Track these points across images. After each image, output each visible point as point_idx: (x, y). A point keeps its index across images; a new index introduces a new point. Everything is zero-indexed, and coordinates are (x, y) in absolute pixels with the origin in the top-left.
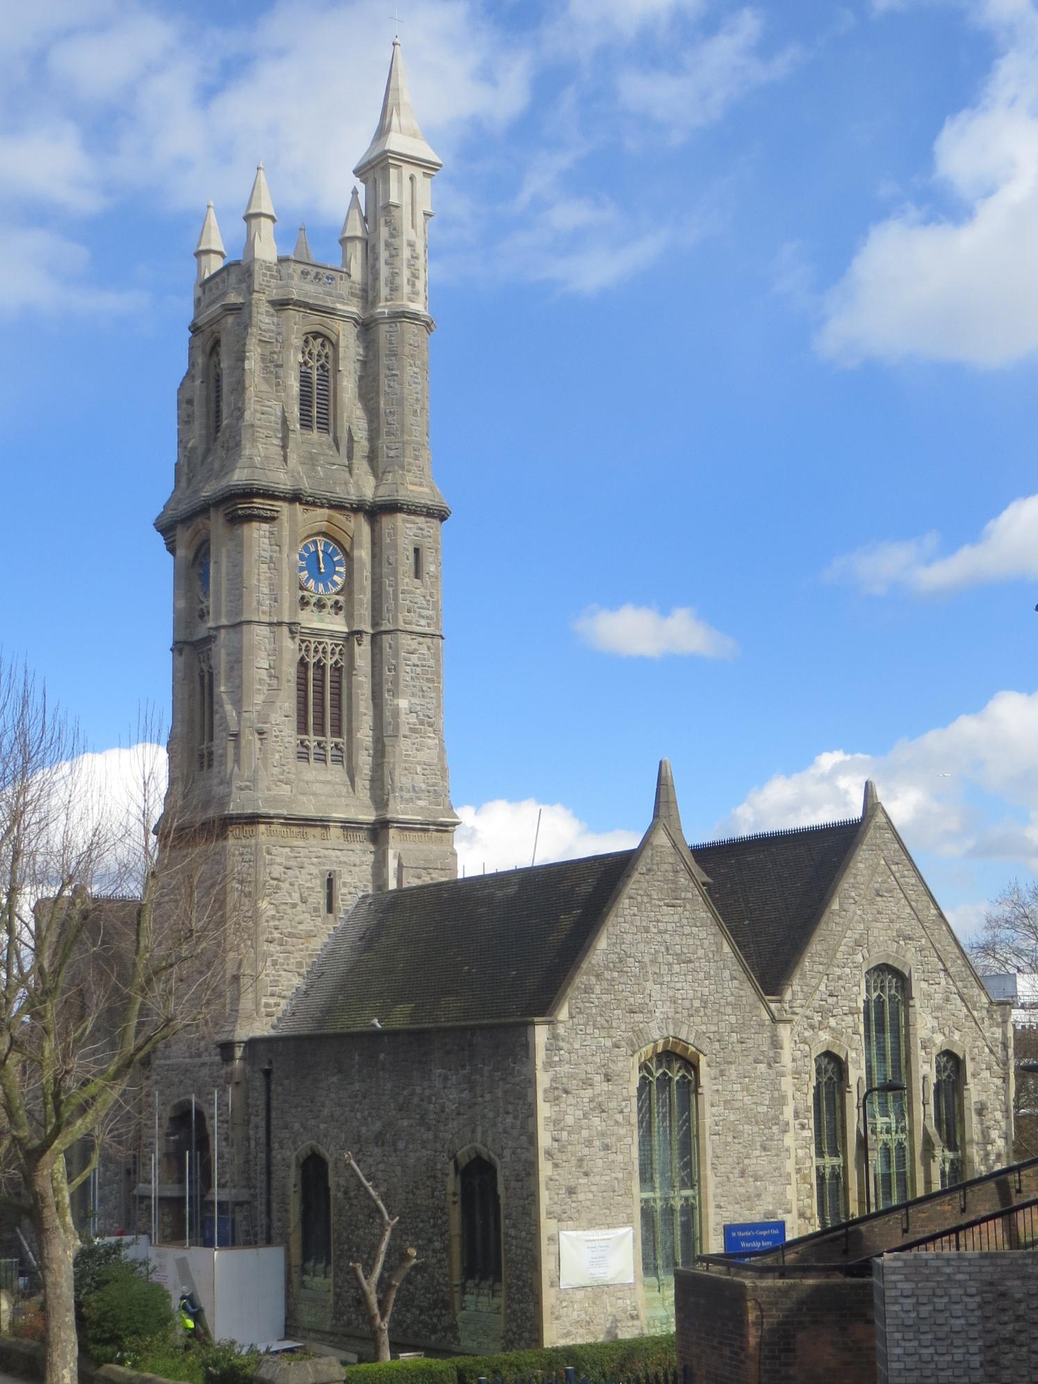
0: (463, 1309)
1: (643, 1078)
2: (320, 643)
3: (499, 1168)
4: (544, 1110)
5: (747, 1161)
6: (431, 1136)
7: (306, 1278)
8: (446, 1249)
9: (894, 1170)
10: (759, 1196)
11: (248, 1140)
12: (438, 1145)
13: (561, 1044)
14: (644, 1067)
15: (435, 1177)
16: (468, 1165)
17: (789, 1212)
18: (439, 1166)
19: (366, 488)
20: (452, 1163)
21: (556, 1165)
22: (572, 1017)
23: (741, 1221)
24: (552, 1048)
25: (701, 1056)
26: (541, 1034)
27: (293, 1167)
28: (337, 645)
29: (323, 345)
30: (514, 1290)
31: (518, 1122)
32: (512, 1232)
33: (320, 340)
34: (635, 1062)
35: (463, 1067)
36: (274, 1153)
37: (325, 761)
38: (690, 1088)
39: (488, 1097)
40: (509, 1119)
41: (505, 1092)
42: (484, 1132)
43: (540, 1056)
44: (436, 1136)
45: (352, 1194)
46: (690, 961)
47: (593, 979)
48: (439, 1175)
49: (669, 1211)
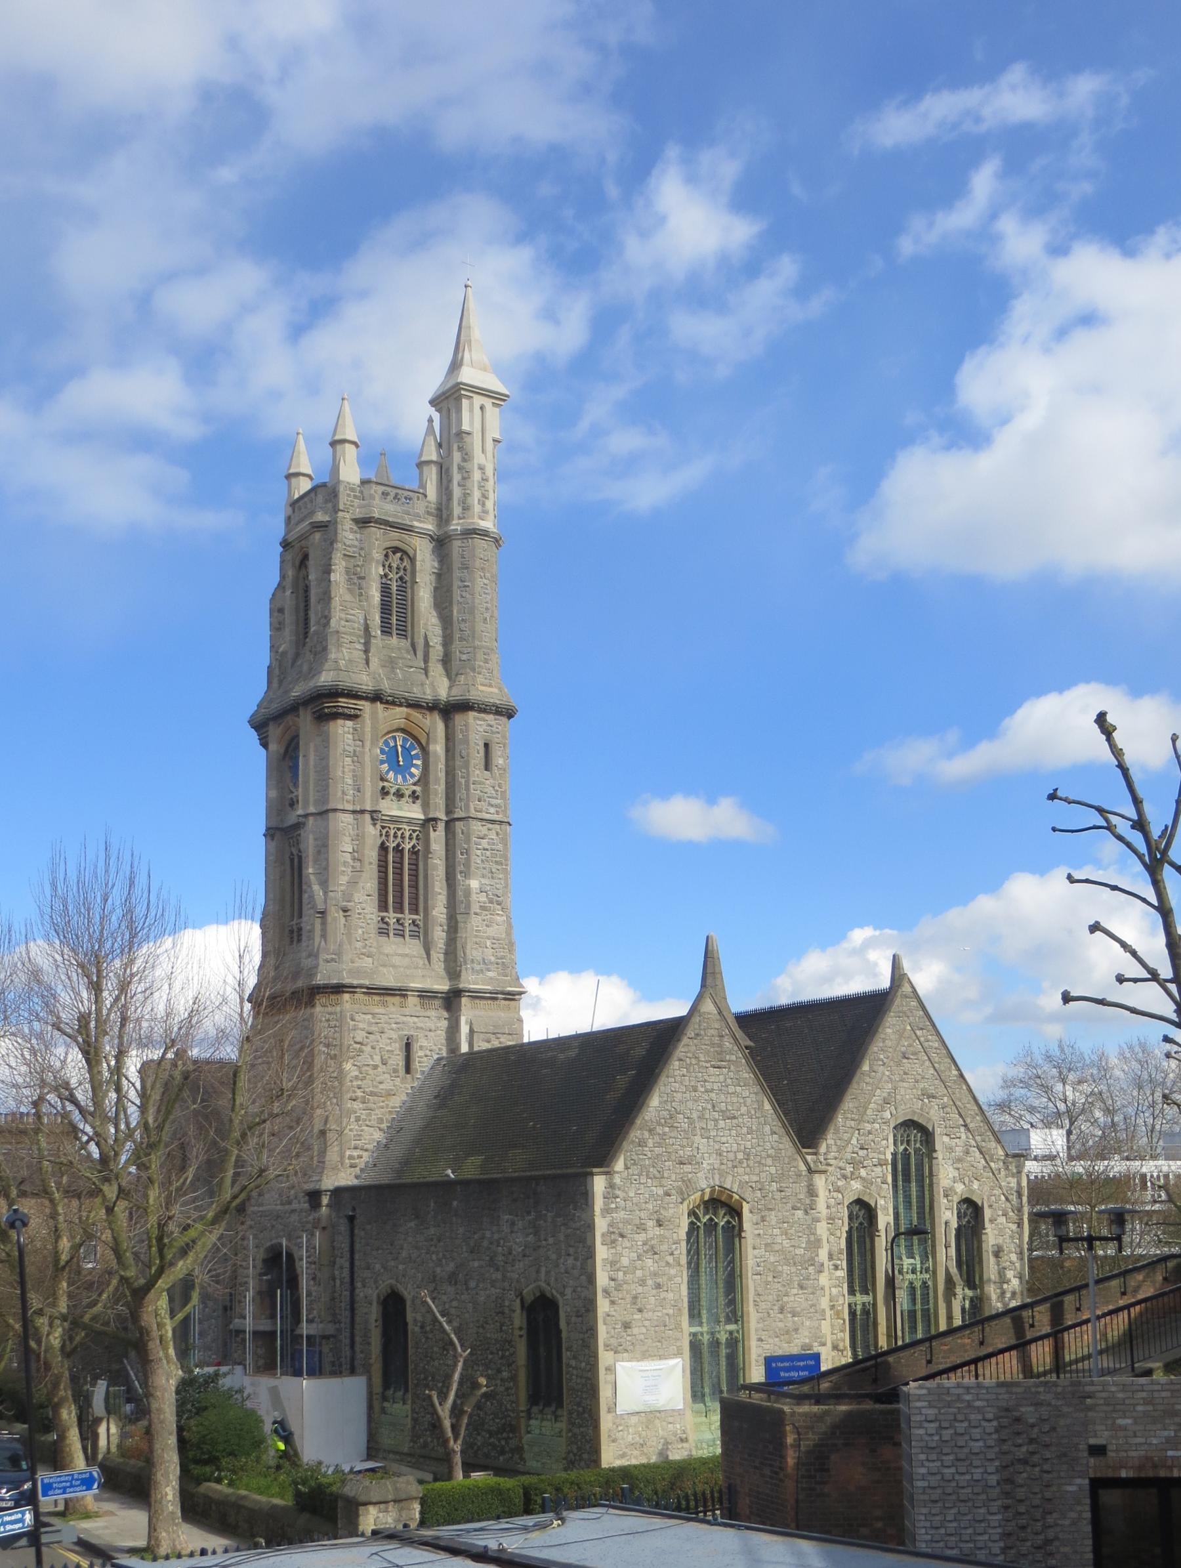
0: (529, 1432)
1: (692, 1223)
2: (399, 829)
3: (561, 1305)
4: (602, 1252)
5: (785, 1299)
6: (499, 1276)
7: (386, 1404)
8: (513, 1378)
9: (918, 1306)
10: (796, 1330)
11: (334, 1279)
12: (506, 1284)
13: (618, 1192)
14: (692, 1213)
15: (503, 1313)
16: (533, 1302)
17: (824, 1345)
18: (507, 1303)
19: (440, 688)
20: (518, 1301)
21: (613, 1303)
22: (627, 1168)
23: (780, 1353)
24: (609, 1196)
25: (744, 1204)
26: (599, 1184)
27: (375, 1304)
28: (414, 831)
29: (401, 559)
30: (574, 1415)
31: (579, 1264)
32: (573, 1363)
33: (399, 555)
34: (684, 1208)
35: (529, 1213)
36: (357, 1291)
37: (403, 936)
38: (734, 1232)
39: (551, 1241)
40: (570, 1261)
41: (567, 1236)
42: (548, 1273)
43: (599, 1203)
44: (504, 1276)
45: (428, 1328)
46: (734, 1118)
47: (646, 1134)
48: (507, 1311)
49: (715, 1344)
